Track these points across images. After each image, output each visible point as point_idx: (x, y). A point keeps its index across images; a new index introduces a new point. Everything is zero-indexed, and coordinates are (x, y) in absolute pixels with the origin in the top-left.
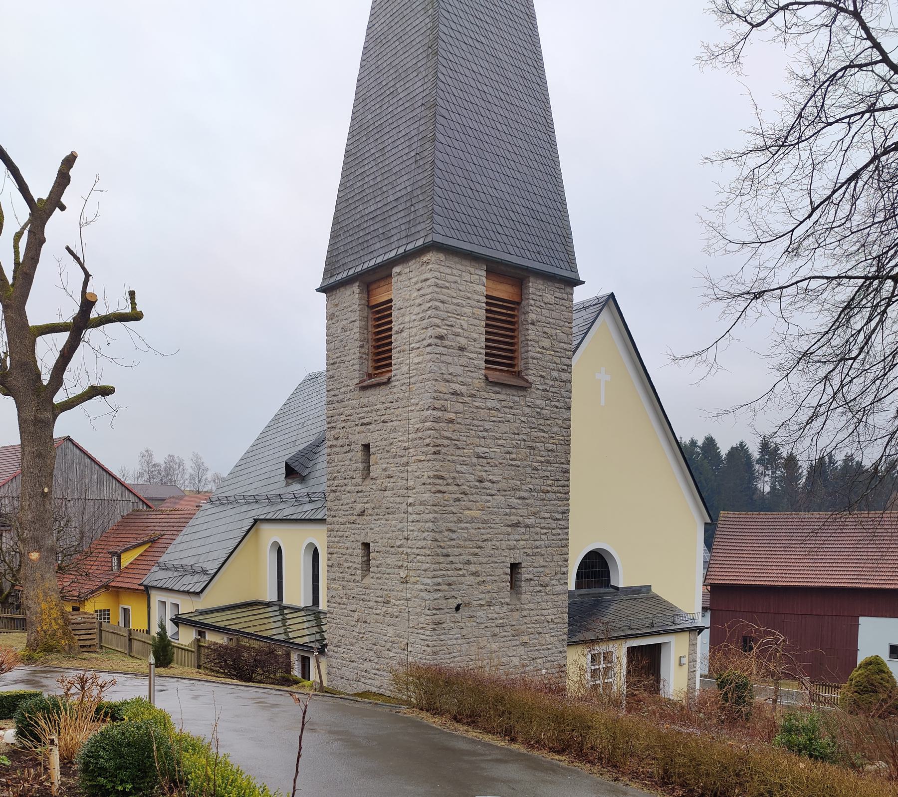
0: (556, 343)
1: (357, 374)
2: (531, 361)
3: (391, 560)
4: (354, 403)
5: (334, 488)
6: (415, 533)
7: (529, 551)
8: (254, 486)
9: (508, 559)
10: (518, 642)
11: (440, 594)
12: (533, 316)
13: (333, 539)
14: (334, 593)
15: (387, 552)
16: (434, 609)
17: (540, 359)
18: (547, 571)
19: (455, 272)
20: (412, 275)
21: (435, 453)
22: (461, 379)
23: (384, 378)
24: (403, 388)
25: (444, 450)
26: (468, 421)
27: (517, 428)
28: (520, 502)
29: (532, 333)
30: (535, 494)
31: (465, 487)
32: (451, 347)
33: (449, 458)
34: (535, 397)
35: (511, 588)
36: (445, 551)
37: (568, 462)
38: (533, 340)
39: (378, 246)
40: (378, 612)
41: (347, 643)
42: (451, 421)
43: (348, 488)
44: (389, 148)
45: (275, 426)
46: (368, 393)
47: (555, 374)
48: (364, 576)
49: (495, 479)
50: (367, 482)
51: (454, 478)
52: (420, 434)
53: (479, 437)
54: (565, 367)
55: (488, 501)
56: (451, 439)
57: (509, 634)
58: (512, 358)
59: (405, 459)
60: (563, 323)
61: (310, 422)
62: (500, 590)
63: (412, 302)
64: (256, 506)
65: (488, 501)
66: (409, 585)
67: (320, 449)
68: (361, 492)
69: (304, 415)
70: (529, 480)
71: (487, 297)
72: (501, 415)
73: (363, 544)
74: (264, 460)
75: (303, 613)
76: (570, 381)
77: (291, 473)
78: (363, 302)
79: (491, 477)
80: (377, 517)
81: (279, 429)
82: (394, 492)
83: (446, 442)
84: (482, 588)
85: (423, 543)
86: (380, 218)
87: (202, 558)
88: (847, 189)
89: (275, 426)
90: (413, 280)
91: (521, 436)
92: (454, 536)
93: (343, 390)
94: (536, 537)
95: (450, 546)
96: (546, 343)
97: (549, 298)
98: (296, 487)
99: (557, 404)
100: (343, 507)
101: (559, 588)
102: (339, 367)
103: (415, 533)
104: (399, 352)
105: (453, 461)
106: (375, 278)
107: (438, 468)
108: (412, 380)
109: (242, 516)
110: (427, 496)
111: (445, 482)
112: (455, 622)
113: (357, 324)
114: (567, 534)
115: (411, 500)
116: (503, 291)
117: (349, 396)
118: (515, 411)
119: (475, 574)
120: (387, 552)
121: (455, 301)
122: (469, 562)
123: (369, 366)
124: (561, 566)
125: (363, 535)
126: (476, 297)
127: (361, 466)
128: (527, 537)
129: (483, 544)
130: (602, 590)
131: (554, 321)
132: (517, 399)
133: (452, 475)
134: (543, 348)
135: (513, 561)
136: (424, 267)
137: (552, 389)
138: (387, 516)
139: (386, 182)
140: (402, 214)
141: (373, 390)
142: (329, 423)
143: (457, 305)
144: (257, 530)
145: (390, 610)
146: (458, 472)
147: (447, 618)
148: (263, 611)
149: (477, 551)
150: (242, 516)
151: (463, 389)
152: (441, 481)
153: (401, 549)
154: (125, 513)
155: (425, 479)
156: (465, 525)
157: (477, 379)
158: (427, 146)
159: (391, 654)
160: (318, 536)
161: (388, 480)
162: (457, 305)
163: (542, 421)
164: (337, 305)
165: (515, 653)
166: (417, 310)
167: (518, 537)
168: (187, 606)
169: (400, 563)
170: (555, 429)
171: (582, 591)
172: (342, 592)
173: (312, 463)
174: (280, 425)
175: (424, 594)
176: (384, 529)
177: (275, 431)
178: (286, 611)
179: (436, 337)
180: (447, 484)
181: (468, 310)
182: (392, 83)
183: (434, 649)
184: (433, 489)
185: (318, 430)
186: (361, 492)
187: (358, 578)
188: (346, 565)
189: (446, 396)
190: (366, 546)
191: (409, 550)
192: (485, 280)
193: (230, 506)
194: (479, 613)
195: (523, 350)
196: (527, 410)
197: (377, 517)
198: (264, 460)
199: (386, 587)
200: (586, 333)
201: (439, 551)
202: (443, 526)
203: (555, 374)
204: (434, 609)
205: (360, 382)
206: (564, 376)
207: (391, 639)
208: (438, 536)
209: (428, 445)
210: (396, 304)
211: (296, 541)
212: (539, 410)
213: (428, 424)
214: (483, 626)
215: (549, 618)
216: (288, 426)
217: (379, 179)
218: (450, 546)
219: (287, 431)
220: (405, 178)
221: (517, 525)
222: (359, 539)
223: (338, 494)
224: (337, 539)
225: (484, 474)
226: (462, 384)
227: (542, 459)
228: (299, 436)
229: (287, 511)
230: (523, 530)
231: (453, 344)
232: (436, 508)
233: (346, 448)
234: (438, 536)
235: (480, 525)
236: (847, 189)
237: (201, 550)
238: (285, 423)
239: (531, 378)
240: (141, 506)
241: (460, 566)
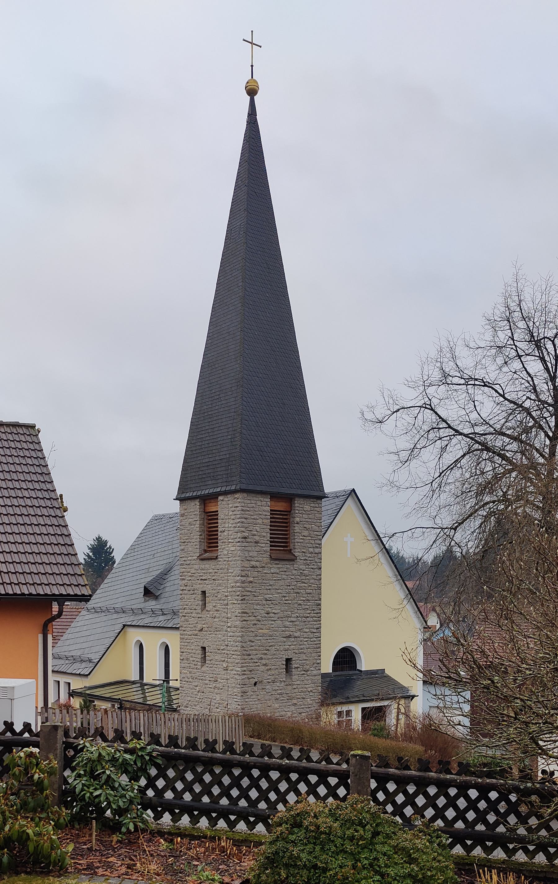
0: (311, 533)
1: (198, 551)
2: (296, 544)
3: (218, 657)
4: (196, 567)
5: (184, 614)
6: (232, 643)
7: (297, 651)
8: (120, 600)
9: (284, 656)
10: (291, 703)
11: (246, 676)
12: (297, 519)
13: (184, 644)
14: (184, 676)
15: (216, 653)
17: (302, 542)
18: (308, 662)
19: (252, 502)
20: (229, 502)
21: (242, 600)
22: (256, 559)
23: (213, 555)
24: (225, 563)
25: (247, 598)
26: (260, 581)
27: (289, 582)
28: (291, 623)
29: (297, 528)
30: (300, 619)
32: (251, 542)
33: (250, 602)
34: (300, 564)
35: (287, 672)
36: (248, 653)
37: (320, 600)
38: (298, 532)
39: (210, 482)
40: (211, 686)
42: (251, 582)
43: (193, 615)
44: (216, 429)
45: (132, 555)
46: (205, 562)
47: (311, 550)
48: (202, 666)
49: (276, 612)
50: (204, 612)
51: (253, 613)
52: (234, 589)
53: (267, 589)
54: (318, 545)
55: (272, 624)
56: (251, 592)
57: (285, 699)
58: (286, 539)
59: (226, 602)
60: (316, 521)
61: (158, 555)
62: (280, 673)
63: (229, 517)
64: (123, 615)
65: (272, 624)
66: (228, 671)
67: (167, 576)
69: (153, 549)
70: (296, 611)
72: (279, 576)
74: (126, 580)
75: (158, 688)
76: (321, 553)
77: (147, 592)
78: (202, 510)
79: (274, 611)
80: (210, 633)
81: (135, 557)
82: (220, 619)
83: (248, 593)
84: (269, 672)
85: (236, 648)
86: (211, 467)
87: (86, 651)
89: (132, 555)
90: (230, 505)
91: (291, 587)
92: (253, 644)
93: (190, 558)
94: (301, 643)
95: (251, 650)
96: (306, 533)
98: (152, 604)
99: (313, 567)
100: (190, 626)
101: (315, 672)
102: (187, 545)
103: (232, 643)
104: (222, 543)
105: (252, 604)
107: (244, 608)
108: (230, 559)
109: (113, 622)
113: (198, 522)
114: (320, 641)
116: (281, 506)
117: (193, 562)
118: (287, 573)
119: (265, 665)
120: (216, 653)
121: (252, 517)
122: (261, 659)
123: (205, 546)
124: (316, 659)
125: (202, 642)
126: (264, 513)
127: (200, 603)
128: (295, 643)
129: (270, 648)
130: (351, 672)
131: (310, 520)
132: (289, 566)
133: (252, 611)
134: (304, 536)
135: (287, 657)
136: (236, 500)
137: (310, 559)
138: (216, 632)
139: (214, 448)
140: (224, 468)
141: (207, 561)
142: (181, 576)
143: (254, 519)
144: (125, 631)
145: (217, 685)
146: (255, 609)
148: (130, 687)
149: (266, 652)
150: (113, 622)
151: (258, 564)
152: (245, 615)
153: (224, 651)
155: (236, 614)
157: (265, 558)
158: (237, 435)
159: (218, 710)
160: (173, 640)
162: (254, 519)
163: (303, 578)
165: (289, 709)
166: (232, 522)
167: (290, 644)
168: (77, 684)
169: (223, 659)
170: (312, 581)
171: (337, 673)
172: (189, 675)
173: (162, 587)
174: (135, 554)
175: (236, 676)
176: (214, 640)
177: (132, 558)
178: (146, 687)
179: (242, 538)
181: (260, 521)
182: (218, 393)
184: (242, 619)
185: (165, 562)
187: (199, 667)
188: (191, 659)
189: (248, 569)
190: (204, 649)
191: (228, 652)
192: (269, 503)
193: (103, 614)
194: (267, 687)
195: (292, 538)
196: (294, 572)
197: (210, 633)
198: (126, 580)
199: (215, 672)
200: (336, 515)
201: (245, 652)
202: (247, 639)
203: (311, 550)
205: (200, 555)
206: (317, 550)
208: (244, 645)
209: (238, 596)
210: (221, 516)
211: (152, 641)
212: (301, 571)
213: (238, 584)
214: (270, 694)
215: (309, 689)
216: (142, 555)
217: (211, 445)
218: (251, 650)
219: (142, 560)
220: (225, 449)
221: (289, 637)
222: (199, 644)
223: (186, 618)
224: (186, 644)
225: (269, 609)
226: (257, 561)
227: (304, 599)
228: (151, 565)
229: (147, 620)
230: (293, 639)
231: (252, 540)
232: (243, 630)
233: (192, 592)
234: (244, 645)
235: (268, 638)
237: (85, 645)
238: (139, 553)
239: (296, 554)
241: (257, 661)
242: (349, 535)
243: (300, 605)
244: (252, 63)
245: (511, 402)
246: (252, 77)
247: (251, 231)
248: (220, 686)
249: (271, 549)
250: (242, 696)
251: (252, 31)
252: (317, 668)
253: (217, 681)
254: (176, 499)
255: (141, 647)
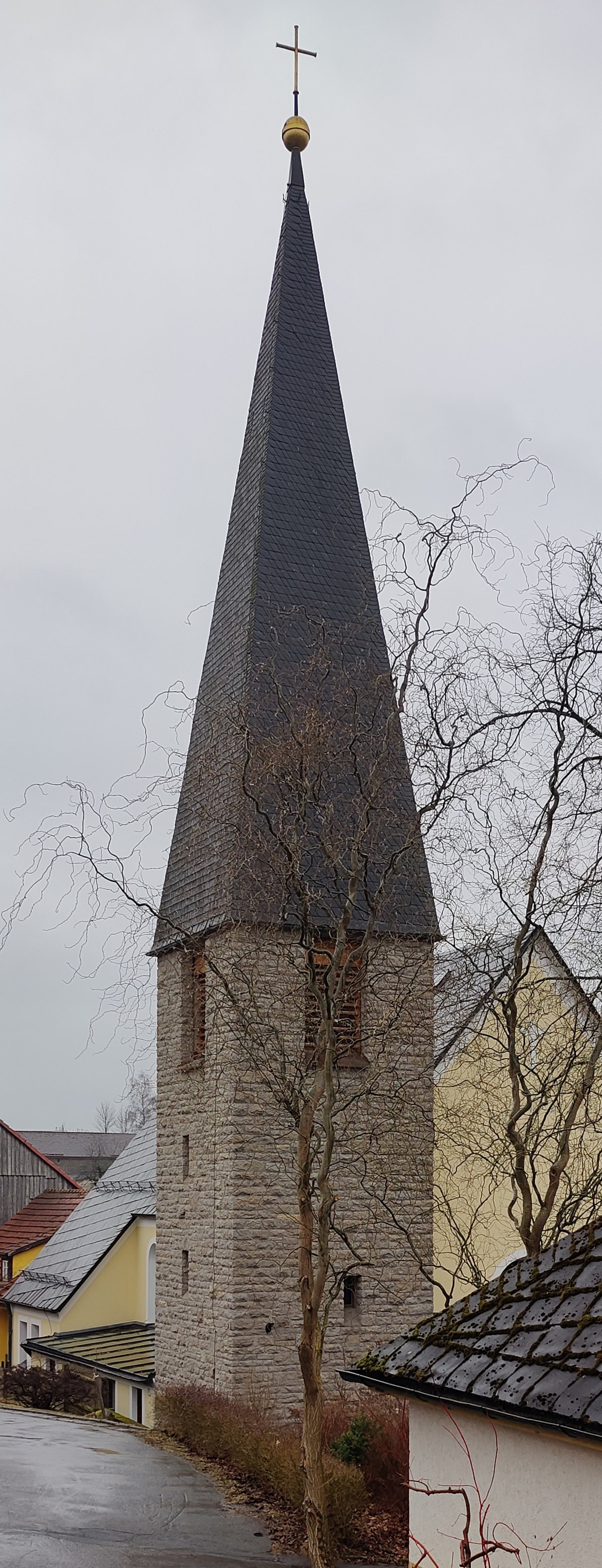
5: (161, 1185)
11: (243, 1312)
16: (236, 1329)
31: (278, 1187)
36: (250, 1262)
41: (170, 1371)
51: (263, 1178)
68: (182, 1190)
73: (184, 1251)
92: (264, 1244)
97: (397, 959)
100: (169, 1208)
105: (262, 1159)
107: (241, 1167)
110: (230, 1199)
111: (251, 1183)
112: (264, 1345)
115: (217, 1203)
144: (137, 1228)
147: (256, 1341)
152: (245, 1182)
154: (37, 1194)
156: (280, 1231)
161: (202, 1178)
164: (165, 973)
175: (227, 1311)
180: (254, 1185)
183: (238, 1376)
186: (182, 1190)
190: (186, 1253)
204: (236, 1329)
207: (204, 1365)
209: (230, 1142)
230: (364, 1236)
240: (60, 1185)
241: (274, 1279)
244: (296, 87)
246: (296, 113)
247: (282, 408)
248: (205, 1331)
249: (306, 1047)
250: (237, 1353)
251: (296, 27)
252: (424, 1299)
253: (201, 1321)
254: (151, 954)
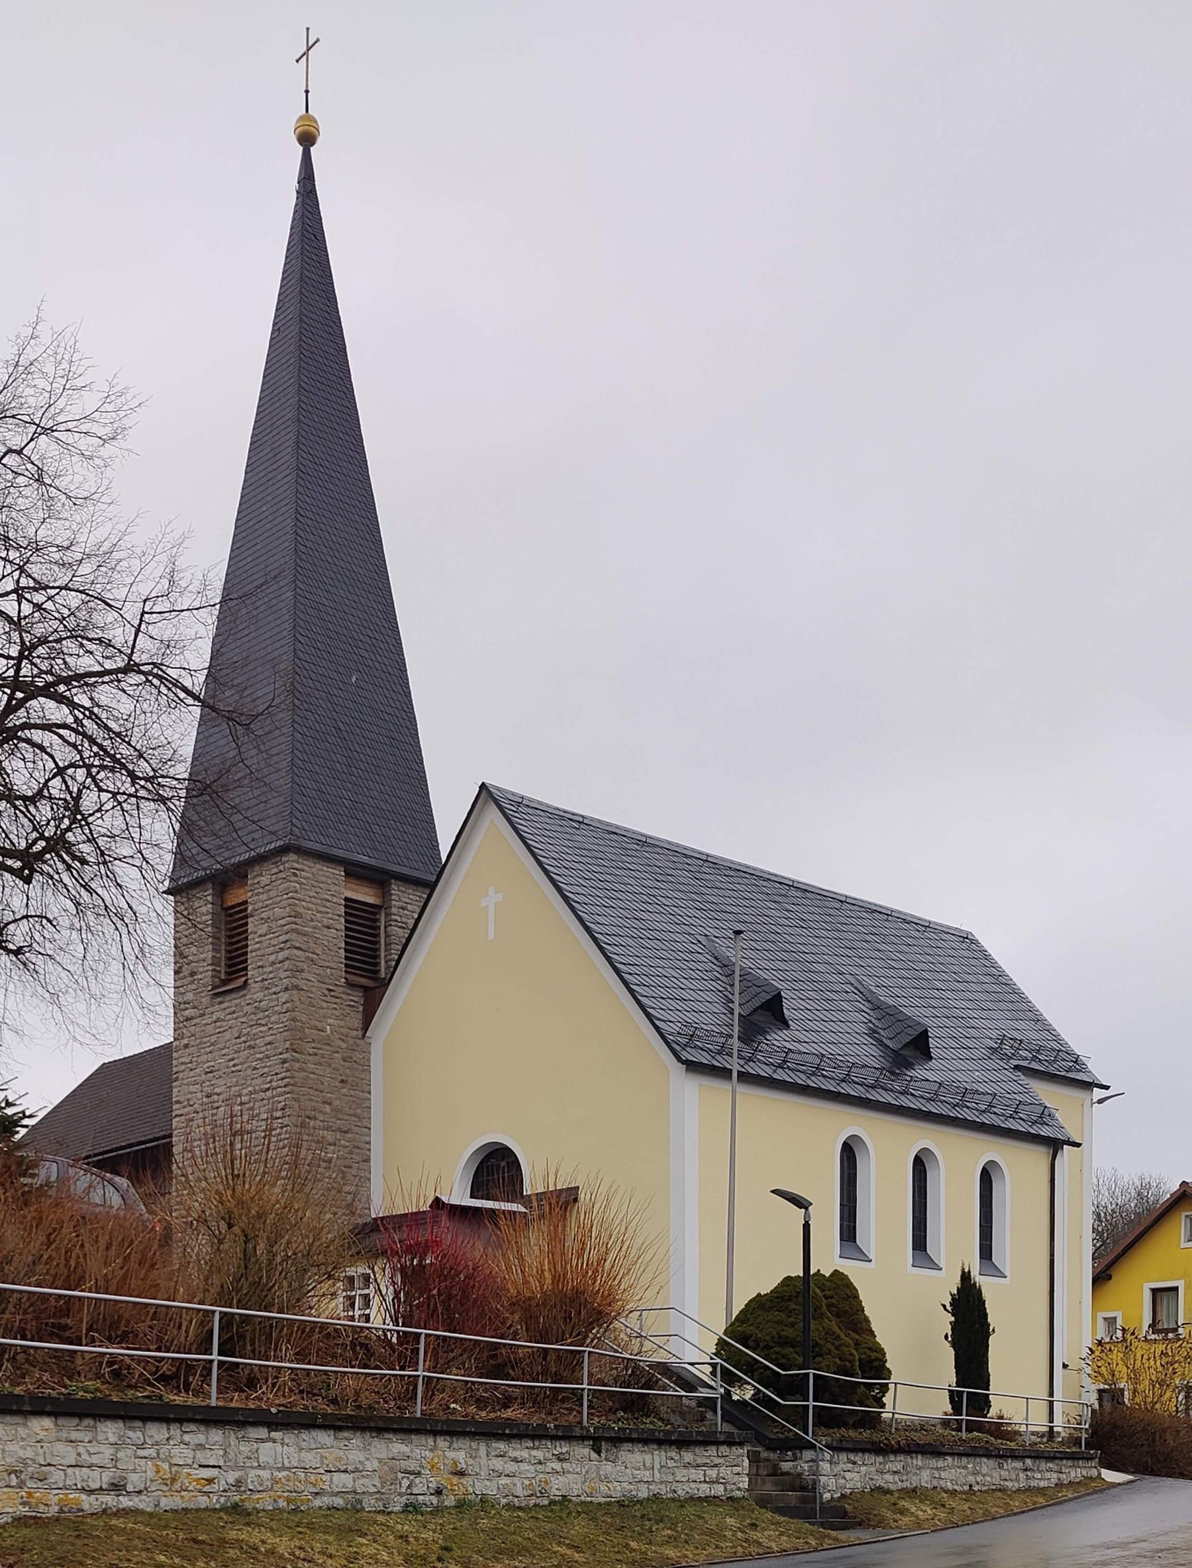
17: (259, 949)
71: (346, 899)
88: (659, 1019)
106: (226, 880)
116: (366, 895)
132: (237, 1001)
196: (246, 1008)
203: (272, 958)
227: (261, 1056)
236: (659, 1019)
242: (491, 890)
243: (255, 1068)
245: (19, 605)
255: (920, 1242)
